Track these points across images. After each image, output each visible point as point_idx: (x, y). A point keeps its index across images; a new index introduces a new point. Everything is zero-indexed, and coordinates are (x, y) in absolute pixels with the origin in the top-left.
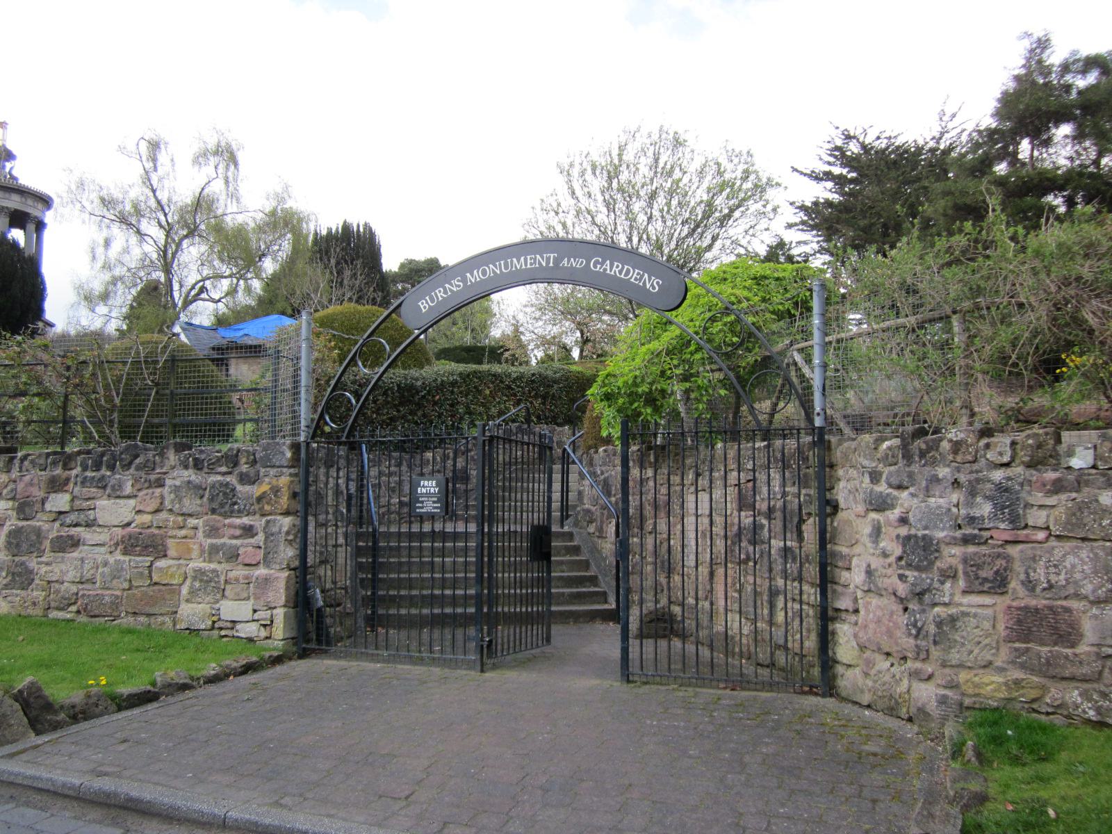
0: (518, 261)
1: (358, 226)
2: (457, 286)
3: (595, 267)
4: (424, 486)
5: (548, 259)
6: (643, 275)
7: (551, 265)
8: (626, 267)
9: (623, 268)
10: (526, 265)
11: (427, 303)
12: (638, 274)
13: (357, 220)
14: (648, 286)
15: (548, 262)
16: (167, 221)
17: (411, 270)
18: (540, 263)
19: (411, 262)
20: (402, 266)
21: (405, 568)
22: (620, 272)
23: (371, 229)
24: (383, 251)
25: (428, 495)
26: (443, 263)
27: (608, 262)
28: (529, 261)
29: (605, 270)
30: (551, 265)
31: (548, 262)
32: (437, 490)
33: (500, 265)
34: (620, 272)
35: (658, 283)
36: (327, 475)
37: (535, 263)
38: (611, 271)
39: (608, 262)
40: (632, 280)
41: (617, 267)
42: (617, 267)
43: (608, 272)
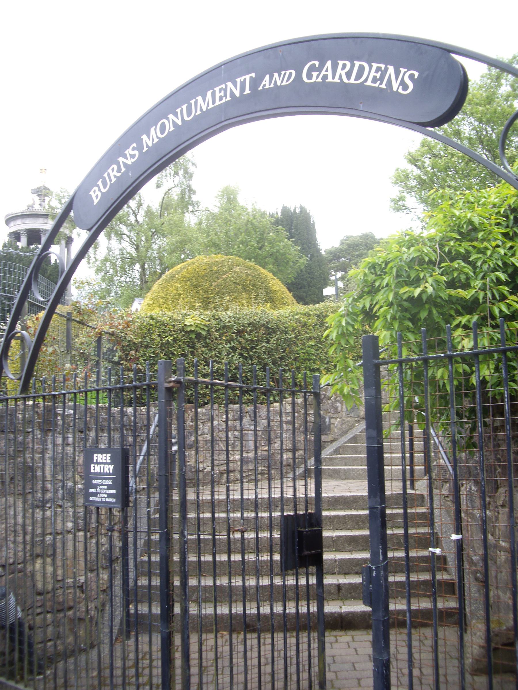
0: (204, 100)
1: (295, 208)
2: (133, 156)
3: (309, 76)
4: (97, 463)
5: (243, 84)
6: (386, 69)
7: (247, 91)
8: (357, 64)
9: (353, 66)
10: (214, 102)
11: (100, 190)
12: (378, 69)
13: (293, 205)
14: (395, 87)
15: (243, 89)
16: (137, 220)
17: (349, 246)
18: (232, 94)
19: (348, 238)
20: (342, 243)
21: (264, 545)
22: (349, 75)
23: (306, 210)
24: (317, 227)
25: (102, 476)
26: (378, 237)
27: (329, 64)
28: (217, 95)
29: (325, 77)
30: (247, 91)
31: (243, 89)
32: (112, 467)
33: (182, 111)
34: (349, 75)
35: (411, 77)
36: (44, 441)
37: (225, 95)
38: (333, 78)
39: (329, 64)
40: (369, 83)
41: (344, 66)
42: (344, 66)
43: (330, 79)
